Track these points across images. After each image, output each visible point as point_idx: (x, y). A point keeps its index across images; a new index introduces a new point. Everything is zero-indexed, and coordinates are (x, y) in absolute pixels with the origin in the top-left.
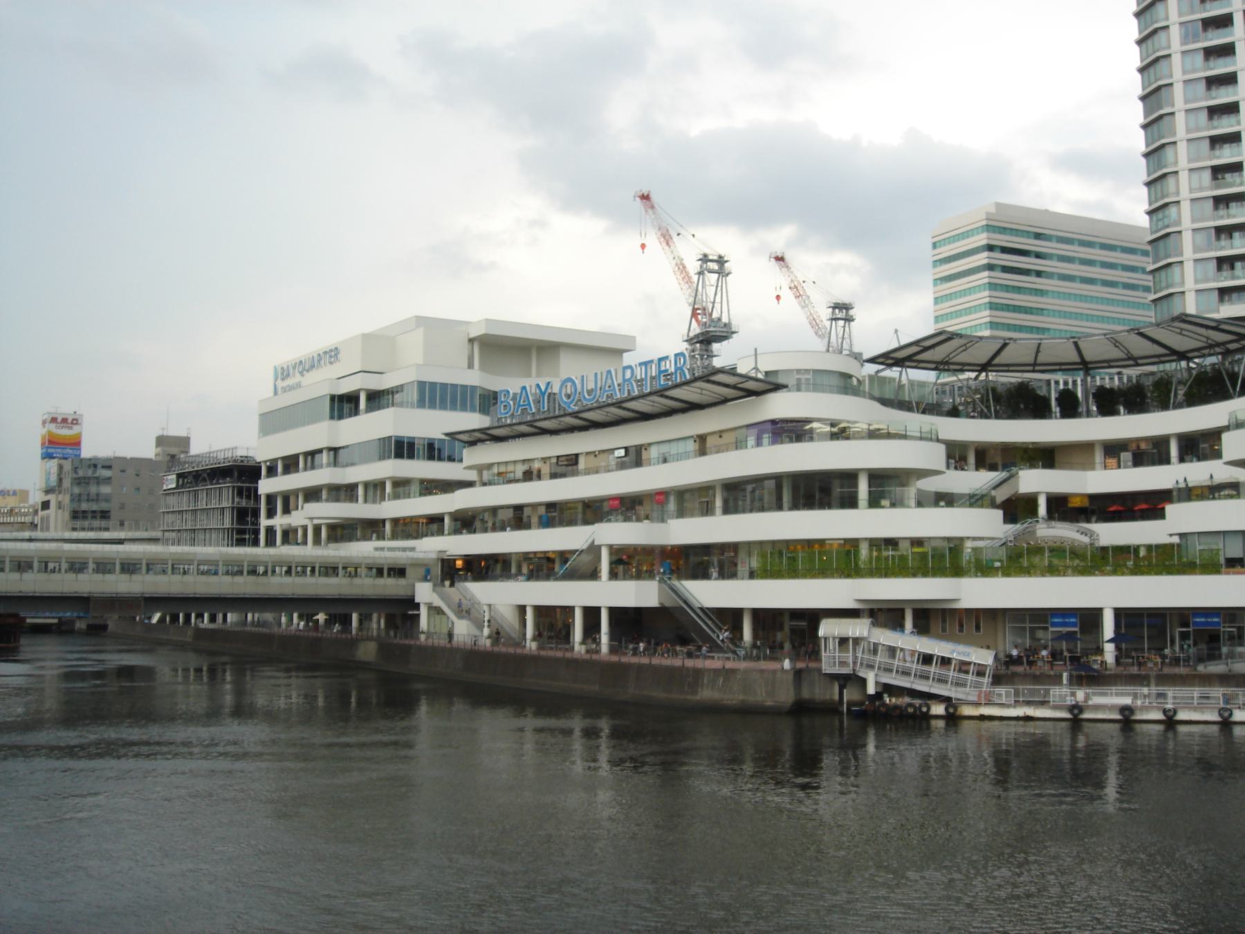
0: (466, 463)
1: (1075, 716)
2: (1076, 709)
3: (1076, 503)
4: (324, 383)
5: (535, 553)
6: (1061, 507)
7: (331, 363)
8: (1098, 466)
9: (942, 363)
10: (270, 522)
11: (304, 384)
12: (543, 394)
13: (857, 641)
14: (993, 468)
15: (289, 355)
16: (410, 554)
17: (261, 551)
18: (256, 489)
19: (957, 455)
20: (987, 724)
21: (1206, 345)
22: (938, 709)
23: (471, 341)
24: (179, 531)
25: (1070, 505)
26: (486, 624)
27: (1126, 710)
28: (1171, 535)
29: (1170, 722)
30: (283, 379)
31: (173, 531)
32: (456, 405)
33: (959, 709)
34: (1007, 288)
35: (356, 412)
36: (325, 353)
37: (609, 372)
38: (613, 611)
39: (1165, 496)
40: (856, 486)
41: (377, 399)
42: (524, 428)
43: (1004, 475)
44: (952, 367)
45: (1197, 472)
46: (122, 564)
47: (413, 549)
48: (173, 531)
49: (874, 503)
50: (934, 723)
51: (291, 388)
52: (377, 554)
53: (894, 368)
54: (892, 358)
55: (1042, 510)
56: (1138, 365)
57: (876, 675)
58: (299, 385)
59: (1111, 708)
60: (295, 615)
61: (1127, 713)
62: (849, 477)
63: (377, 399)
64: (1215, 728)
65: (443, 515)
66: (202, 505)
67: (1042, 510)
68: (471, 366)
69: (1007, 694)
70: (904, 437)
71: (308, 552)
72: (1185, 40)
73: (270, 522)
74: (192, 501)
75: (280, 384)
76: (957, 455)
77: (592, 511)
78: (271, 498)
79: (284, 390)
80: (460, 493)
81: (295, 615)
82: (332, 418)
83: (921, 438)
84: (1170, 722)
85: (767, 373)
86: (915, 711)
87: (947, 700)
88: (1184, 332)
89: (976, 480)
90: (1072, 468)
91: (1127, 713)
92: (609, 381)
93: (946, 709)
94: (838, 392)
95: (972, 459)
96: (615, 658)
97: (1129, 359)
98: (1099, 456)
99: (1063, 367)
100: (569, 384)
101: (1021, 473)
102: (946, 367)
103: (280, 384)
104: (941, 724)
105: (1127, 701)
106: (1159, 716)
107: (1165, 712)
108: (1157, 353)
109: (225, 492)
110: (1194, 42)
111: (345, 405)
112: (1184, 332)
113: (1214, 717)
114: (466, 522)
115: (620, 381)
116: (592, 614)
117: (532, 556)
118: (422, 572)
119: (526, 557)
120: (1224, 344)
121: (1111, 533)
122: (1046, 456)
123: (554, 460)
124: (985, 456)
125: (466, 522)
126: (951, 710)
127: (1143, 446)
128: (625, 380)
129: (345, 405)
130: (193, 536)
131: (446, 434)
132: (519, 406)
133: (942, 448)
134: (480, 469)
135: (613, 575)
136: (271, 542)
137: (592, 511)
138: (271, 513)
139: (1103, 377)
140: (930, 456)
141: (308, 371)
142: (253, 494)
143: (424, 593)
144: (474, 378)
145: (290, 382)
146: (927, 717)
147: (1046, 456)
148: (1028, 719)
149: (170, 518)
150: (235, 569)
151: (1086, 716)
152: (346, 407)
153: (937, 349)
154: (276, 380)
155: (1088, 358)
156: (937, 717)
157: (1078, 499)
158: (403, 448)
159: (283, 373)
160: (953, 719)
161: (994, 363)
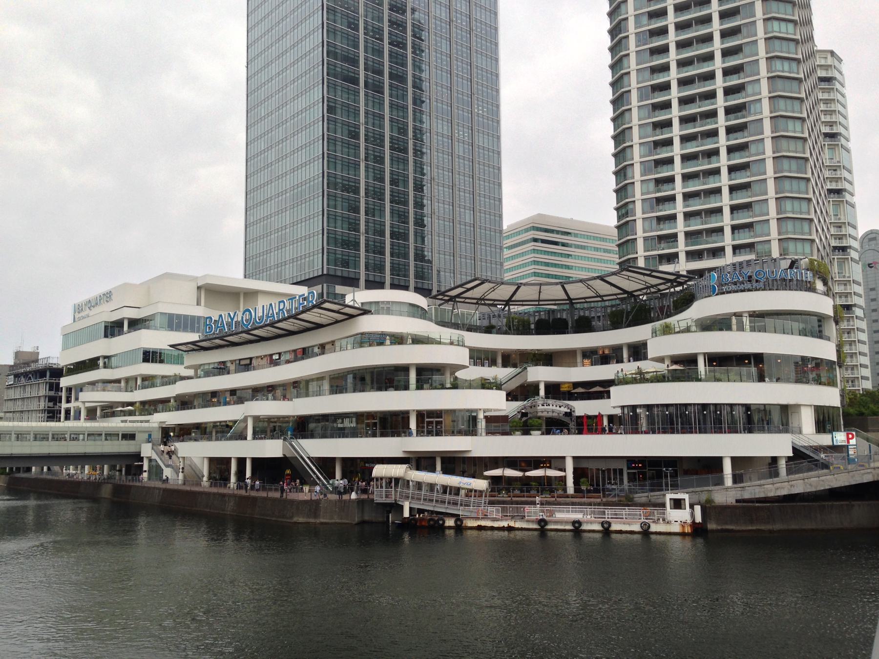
0: (186, 364)
1: (542, 527)
2: (542, 522)
3: (564, 388)
4: (107, 314)
5: (220, 422)
6: (554, 390)
7: (107, 301)
8: (579, 364)
9: (480, 299)
10: (68, 405)
11: (91, 314)
12: (232, 319)
13: (397, 480)
14: (515, 366)
15: (83, 297)
16: (146, 425)
17: (63, 425)
18: (58, 384)
19: (480, 357)
20: (484, 534)
21: (645, 286)
22: (450, 522)
23: (199, 288)
24: (14, 412)
25: (562, 389)
26: (181, 470)
27: (577, 524)
28: (614, 407)
29: (607, 531)
30: (79, 312)
31: (10, 412)
32: (187, 327)
33: (464, 522)
34: (541, 252)
35: (121, 333)
36: (104, 295)
37: (271, 305)
38: (254, 460)
39: (611, 383)
40: (408, 375)
41: (135, 324)
42: (218, 342)
43: (518, 370)
44: (487, 302)
45: (629, 368)
46: (53, 435)
47: (148, 421)
48: (10, 412)
49: (420, 387)
50: (448, 532)
51: (84, 318)
52: (123, 425)
53: (450, 303)
54: (448, 296)
55: (542, 392)
56: (603, 301)
57: (410, 503)
58: (88, 316)
59: (566, 522)
60: (106, 467)
61: (577, 525)
62: (404, 369)
63: (135, 324)
64: (598, 536)
65: (170, 398)
66: (27, 395)
67: (542, 392)
68: (198, 304)
69: (497, 511)
70: (440, 343)
71: (83, 424)
72: (641, 99)
73: (68, 405)
74: (22, 392)
75: (77, 315)
76: (480, 357)
77: (236, 396)
78: (69, 390)
79: (80, 319)
80: (179, 384)
81: (106, 467)
82: (106, 336)
83: (452, 343)
84: (607, 531)
85: (362, 304)
86: (435, 523)
87: (457, 517)
88: (630, 278)
89: (501, 373)
90: (561, 366)
91: (543, 524)
92: (271, 311)
93: (456, 522)
94: (409, 316)
95: (499, 361)
96: (214, 490)
97: (597, 297)
98: (579, 358)
99: (557, 302)
100: (248, 313)
101: (528, 368)
102: (483, 302)
103: (77, 315)
104: (451, 533)
105: (578, 516)
106: (598, 527)
107: (602, 524)
108: (614, 293)
109: (41, 386)
110: (646, 100)
111: (113, 329)
112: (630, 278)
113: (636, 528)
114: (185, 402)
115: (277, 310)
116: (241, 461)
117: (218, 424)
118: (146, 436)
119: (215, 424)
120: (656, 285)
121: (583, 408)
122: (547, 358)
123: (238, 362)
124: (508, 359)
125: (185, 402)
126: (459, 523)
127: (607, 352)
128: (280, 310)
129: (113, 329)
130: (21, 414)
131: (171, 346)
132: (218, 327)
133: (467, 350)
134: (196, 368)
135: (254, 438)
136: (67, 418)
137: (236, 396)
138: (68, 401)
139: (831, 329)
140: (460, 356)
141: (94, 307)
142: (56, 387)
143: (147, 451)
144: (200, 311)
145: (83, 314)
146: (443, 528)
147: (547, 358)
148: (510, 529)
149: (10, 404)
150: (41, 437)
151: (549, 527)
152: (116, 330)
153: (475, 289)
154: (75, 312)
155: (572, 297)
156: (450, 528)
157: (566, 385)
158: (150, 356)
159: (78, 309)
160: (459, 528)
161: (513, 299)
